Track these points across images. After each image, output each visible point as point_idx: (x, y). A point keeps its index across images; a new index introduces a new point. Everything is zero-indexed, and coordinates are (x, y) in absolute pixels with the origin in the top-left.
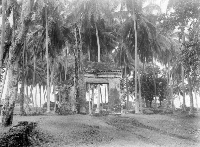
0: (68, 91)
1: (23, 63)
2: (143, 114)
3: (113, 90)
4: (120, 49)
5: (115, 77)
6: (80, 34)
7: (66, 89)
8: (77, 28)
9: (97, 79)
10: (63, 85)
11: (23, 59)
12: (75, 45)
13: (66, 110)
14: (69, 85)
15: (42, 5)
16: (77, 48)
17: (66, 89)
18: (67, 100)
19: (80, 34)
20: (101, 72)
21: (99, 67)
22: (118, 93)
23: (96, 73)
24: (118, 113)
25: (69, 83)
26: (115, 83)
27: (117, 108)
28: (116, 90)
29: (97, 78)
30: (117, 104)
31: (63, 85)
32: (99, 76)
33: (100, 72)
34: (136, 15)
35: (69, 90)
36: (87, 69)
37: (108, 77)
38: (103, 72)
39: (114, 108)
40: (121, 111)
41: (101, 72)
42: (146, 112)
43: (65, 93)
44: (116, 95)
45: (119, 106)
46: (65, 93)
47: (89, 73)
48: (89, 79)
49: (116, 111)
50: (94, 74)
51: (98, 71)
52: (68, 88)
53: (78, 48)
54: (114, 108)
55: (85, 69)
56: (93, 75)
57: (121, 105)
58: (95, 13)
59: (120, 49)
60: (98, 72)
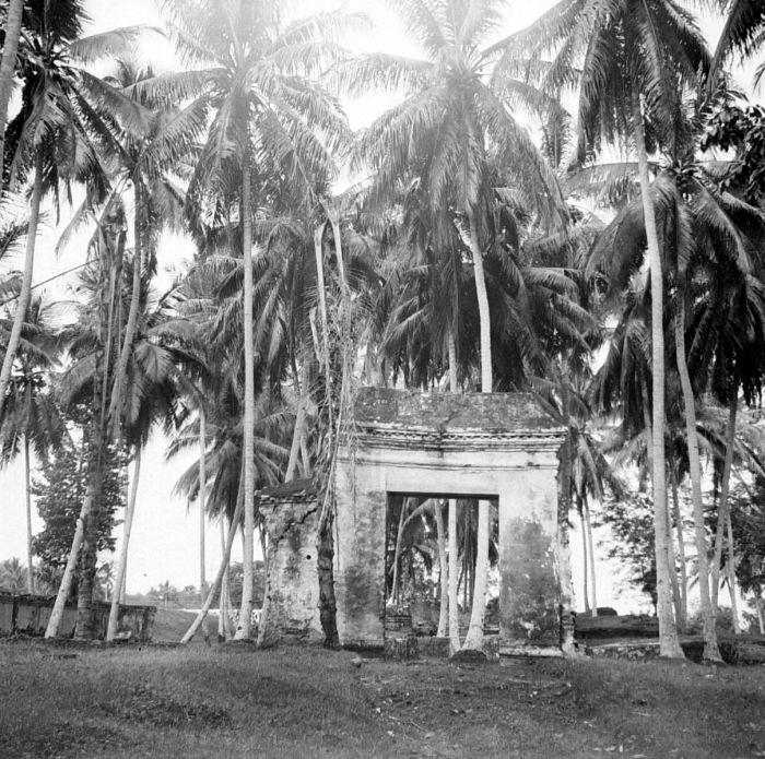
0: (298, 531)
1: (101, 399)
2: (717, 664)
3: (523, 530)
4: (621, 349)
5: (530, 464)
6: (339, 252)
7: (292, 521)
8: (329, 224)
9: (439, 474)
10: (277, 501)
11: (101, 382)
12: (316, 305)
13: (289, 625)
14: (304, 502)
15: (217, 148)
16: (324, 318)
17: (292, 521)
18: (291, 578)
19: (339, 252)
20: (461, 440)
21: (453, 415)
22: (548, 545)
23: (432, 443)
24: (544, 652)
25: (303, 493)
26: (532, 495)
27: (540, 623)
28: (536, 528)
29: (441, 467)
30: (541, 600)
31: (277, 501)
32: (450, 458)
33: (452, 440)
34: (671, 177)
35: (302, 528)
36: (389, 426)
37: (494, 464)
38: (468, 440)
39: (528, 625)
40: (562, 641)
41: (461, 440)
42: (741, 654)
43: (285, 542)
44: (538, 555)
45: (551, 612)
46: (285, 542)
47: (400, 446)
48: (413, 472)
49: (538, 639)
50: (427, 449)
51: (443, 434)
52: (298, 516)
53: (330, 321)
54: (528, 625)
55: (382, 425)
56: (420, 456)
57: (561, 607)
58: (461, 174)
59: (621, 349)
60: (446, 437)
